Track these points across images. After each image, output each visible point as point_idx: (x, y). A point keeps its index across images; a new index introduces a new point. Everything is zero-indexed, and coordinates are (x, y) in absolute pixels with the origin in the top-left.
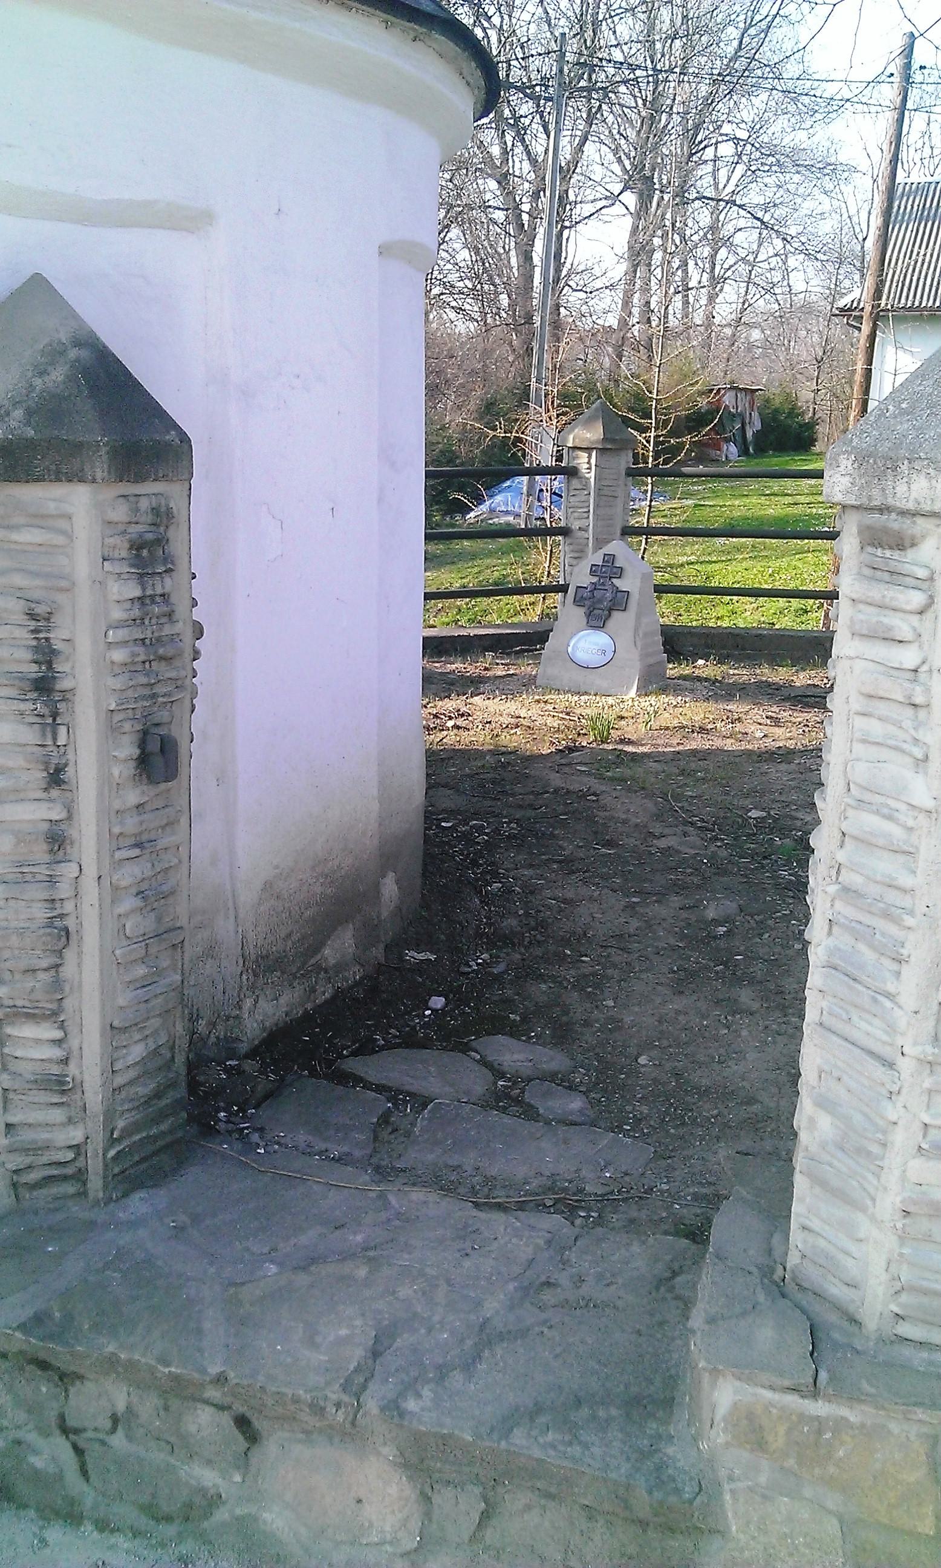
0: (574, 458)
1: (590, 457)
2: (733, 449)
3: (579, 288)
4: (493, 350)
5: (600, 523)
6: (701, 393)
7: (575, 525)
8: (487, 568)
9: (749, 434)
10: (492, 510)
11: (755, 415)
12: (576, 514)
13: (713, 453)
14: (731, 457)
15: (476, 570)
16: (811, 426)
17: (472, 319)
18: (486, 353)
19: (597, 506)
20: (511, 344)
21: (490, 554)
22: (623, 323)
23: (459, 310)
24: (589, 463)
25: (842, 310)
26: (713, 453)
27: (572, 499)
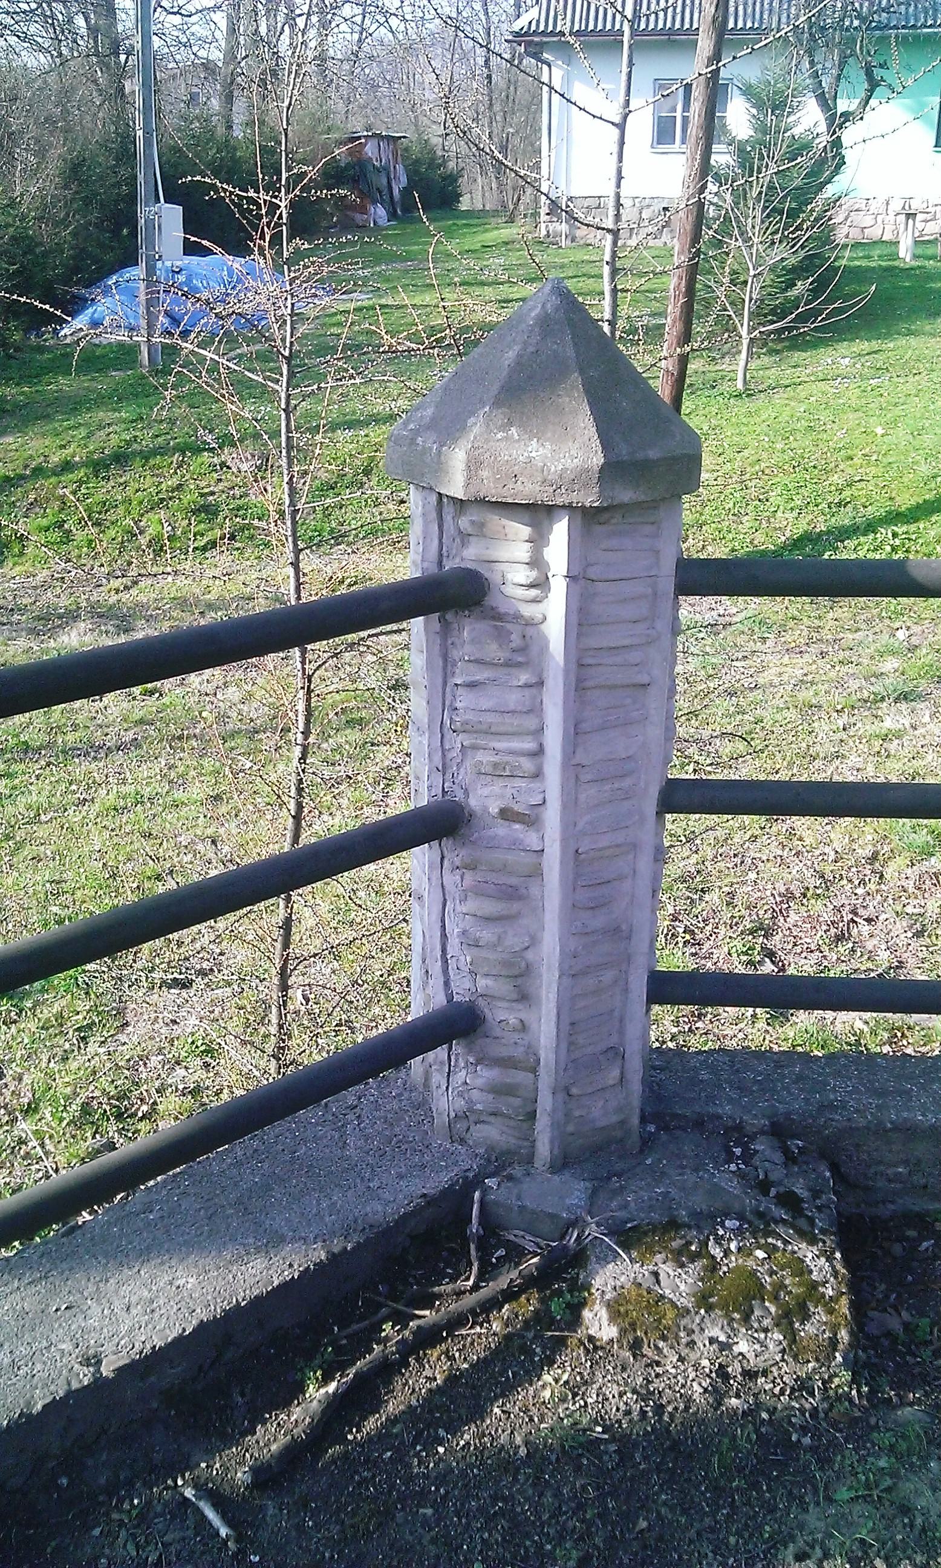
0: (464, 537)
1: (538, 541)
2: (381, 211)
3: (175, 10)
4: (74, 89)
5: (588, 794)
6: (340, 143)
7: (485, 798)
8: (100, 428)
9: (396, 192)
10: (95, 324)
11: (400, 168)
12: (485, 758)
13: (359, 218)
14: (380, 222)
15: (83, 432)
16: (452, 179)
17: (41, 49)
18: (66, 93)
19: (576, 733)
20: (95, 82)
21: (101, 401)
22: (231, 56)
23: (24, 38)
24: (537, 562)
25: (517, 34)
26: (359, 218)
27: (464, 700)
